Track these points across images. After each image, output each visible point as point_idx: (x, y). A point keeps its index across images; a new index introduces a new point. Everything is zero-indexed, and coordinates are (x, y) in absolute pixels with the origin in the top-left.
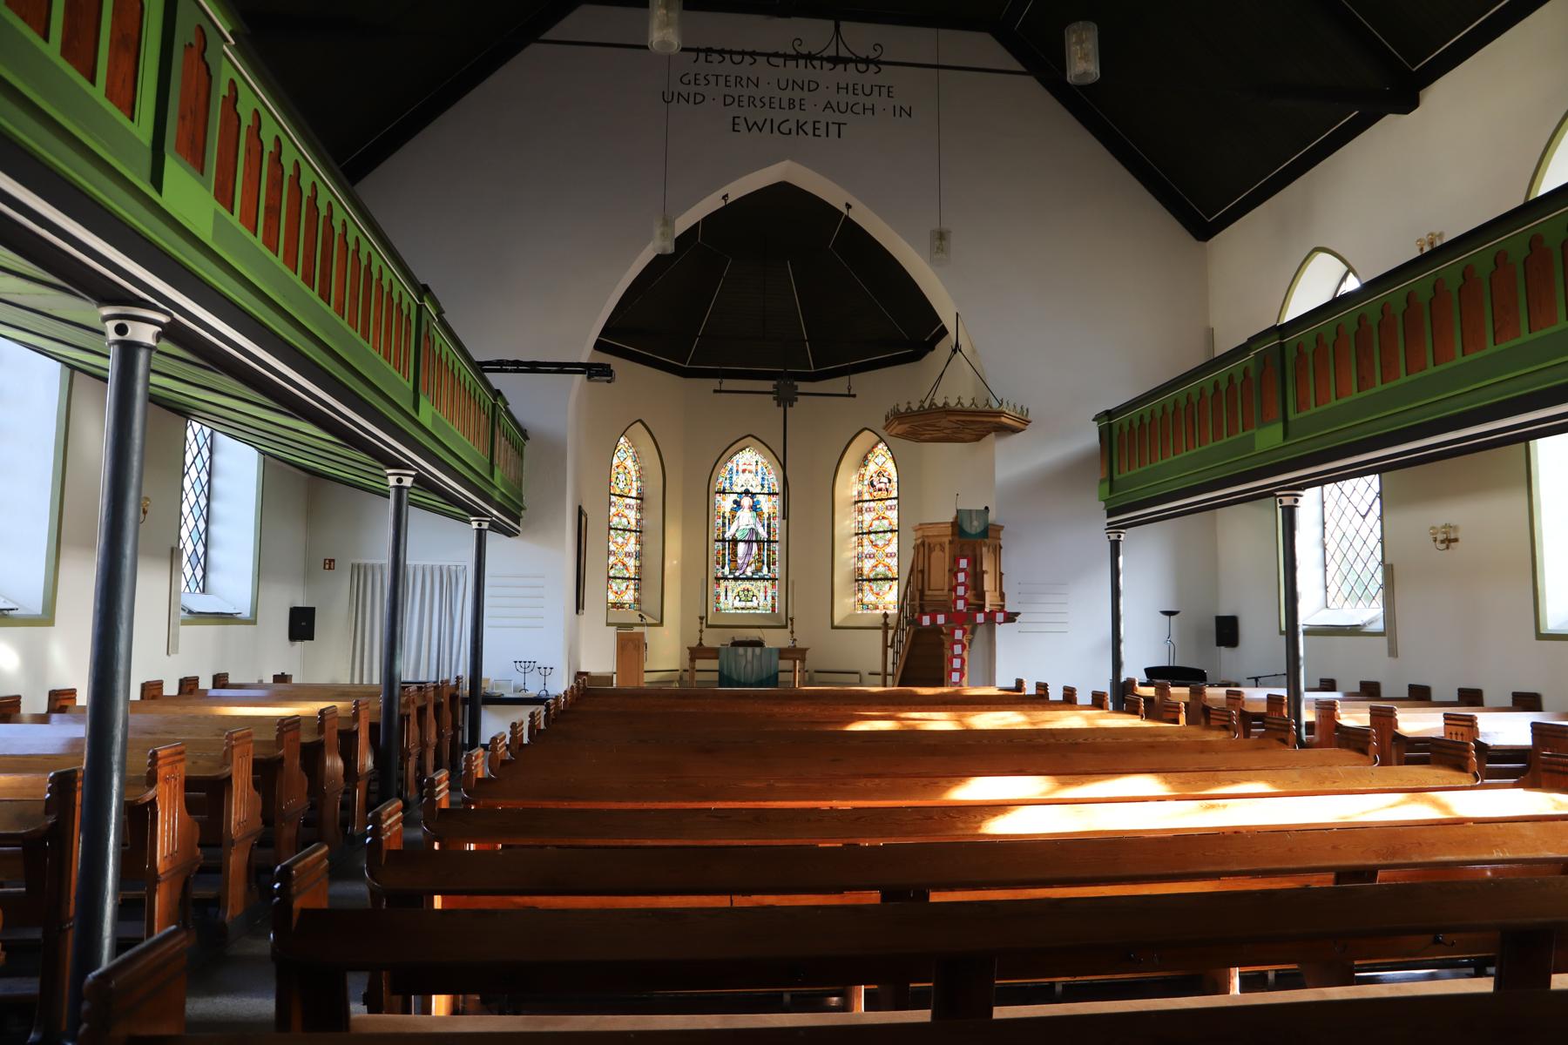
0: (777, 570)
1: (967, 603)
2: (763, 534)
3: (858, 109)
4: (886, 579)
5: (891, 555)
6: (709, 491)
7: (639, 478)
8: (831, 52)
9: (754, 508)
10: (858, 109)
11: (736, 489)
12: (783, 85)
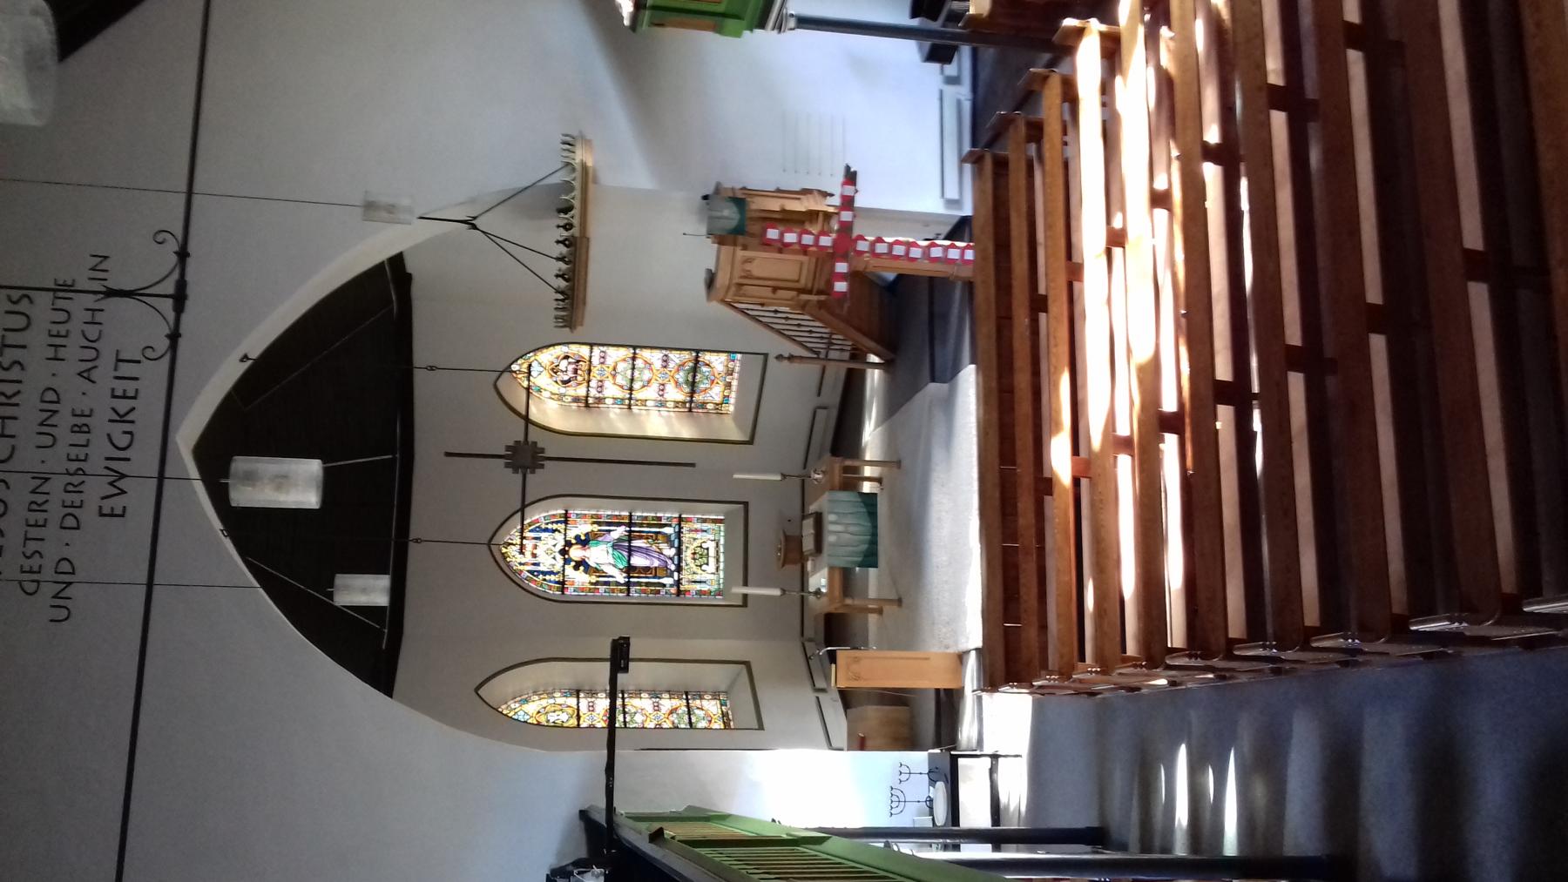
0: (668, 514)
1: (824, 233)
2: (619, 532)
3: (92, 332)
4: (695, 370)
5: (666, 361)
6: (562, 598)
7: (550, 695)
8: (167, 306)
9: (584, 542)
10: (92, 332)
11: (558, 566)
12: (48, 440)
